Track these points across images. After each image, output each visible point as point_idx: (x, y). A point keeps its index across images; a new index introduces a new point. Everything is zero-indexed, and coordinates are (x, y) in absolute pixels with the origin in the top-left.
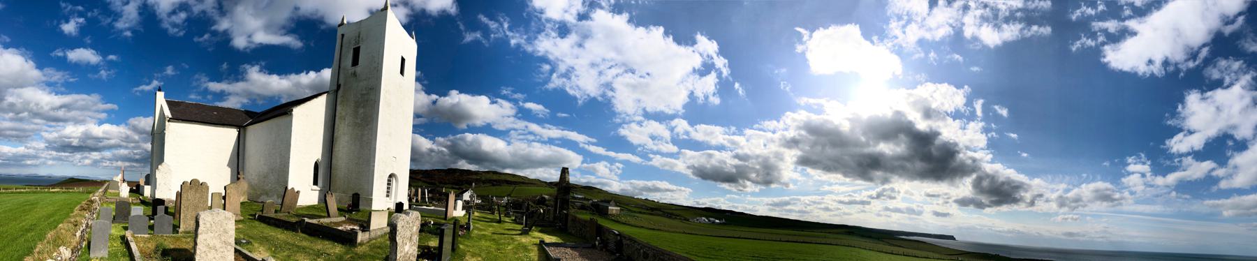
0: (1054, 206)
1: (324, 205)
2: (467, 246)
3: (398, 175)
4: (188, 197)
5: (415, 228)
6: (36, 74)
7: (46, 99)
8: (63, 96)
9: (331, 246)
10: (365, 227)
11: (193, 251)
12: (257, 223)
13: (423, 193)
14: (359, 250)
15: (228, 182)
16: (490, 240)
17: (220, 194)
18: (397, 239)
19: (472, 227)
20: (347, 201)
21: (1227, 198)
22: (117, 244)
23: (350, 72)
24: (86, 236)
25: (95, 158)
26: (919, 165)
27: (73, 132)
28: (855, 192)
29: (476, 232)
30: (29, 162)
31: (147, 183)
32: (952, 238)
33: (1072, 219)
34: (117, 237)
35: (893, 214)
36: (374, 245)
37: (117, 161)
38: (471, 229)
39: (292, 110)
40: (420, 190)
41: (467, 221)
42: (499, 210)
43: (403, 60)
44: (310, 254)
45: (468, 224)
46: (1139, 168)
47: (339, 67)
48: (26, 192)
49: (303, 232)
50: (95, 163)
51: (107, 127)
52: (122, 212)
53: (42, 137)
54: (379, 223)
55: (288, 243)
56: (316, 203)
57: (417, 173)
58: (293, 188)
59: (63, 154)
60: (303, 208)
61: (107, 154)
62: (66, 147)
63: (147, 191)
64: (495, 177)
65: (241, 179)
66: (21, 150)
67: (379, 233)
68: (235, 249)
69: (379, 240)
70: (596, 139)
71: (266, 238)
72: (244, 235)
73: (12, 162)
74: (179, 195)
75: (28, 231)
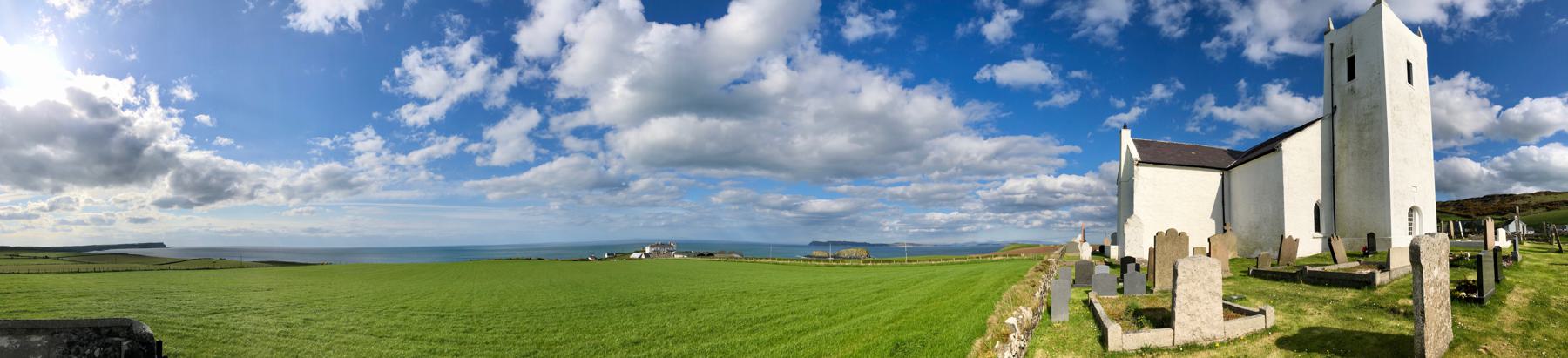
0: (281, 198)
3: (1421, 208)
4: (1166, 248)
6: (956, 115)
7: (975, 148)
8: (996, 139)
10: (1385, 267)
11: (1170, 310)
12: (1251, 279)
13: (1456, 226)
14: (1379, 292)
15: (1213, 232)
16: (1547, 272)
17: (1203, 249)
20: (1363, 242)
21: (487, 179)
22: (1079, 308)
24: (1045, 300)
25: (1049, 218)
26: (101, 169)
27: (1019, 186)
28: (16, 203)
29: (1526, 262)
30: (964, 229)
31: (1114, 242)
32: (161, 245)
33: (308, 212)
34: (1078, 301)
35: (73, 227)
36: (1398, 288)
37: (1078, 221)
38: (1519, 260)
40: (1452, 223)
41: (1512, 250)
42: (1557, 239)
44: (1313, 302)
46: (370, 144)
48: (968, 263)
49: (1305, 282)
50: (1048, 224)
51: (1064, 179)
52: (1083, 275)
53: (978, 197)
54: (1400, 261)
55: (1290, 294)
56: (1320, 252)
58: (1290, 237)
59: (1002, 215)
60: (1303, 259)
61: (1065, 213)
62: (1008, 205)
63: (1114, 252)
64: (1549, 199)
65: (1228, 232)
66: (955, 214)
67: (1402, 273)
68: (1224, 304)
70: (1081, 146)
71: (1263, 292)
72: (1235, 291)
73: (947, 231)
74: (1153, 252)
75: (979, 300)
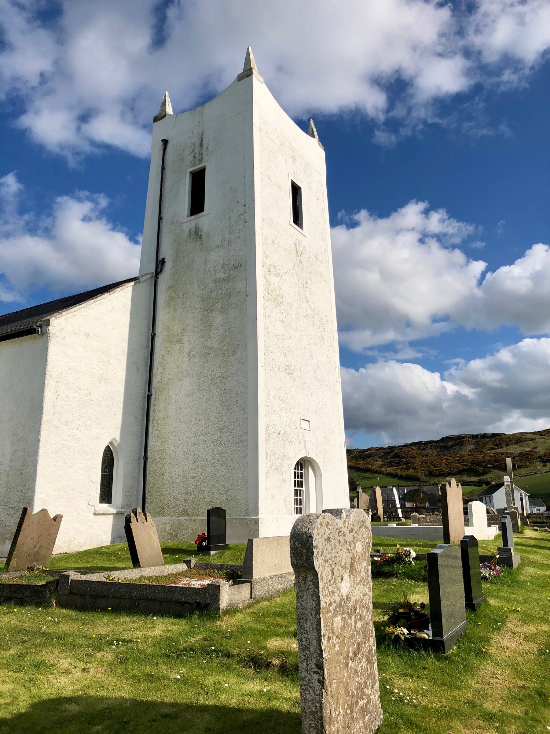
1: (126, 545)
2: (508, 601)
5: (359, 547)
9: (141, 623)
18: (316, 564)
19: (516, 559)
23: (186, 228)
29: (531, 570)
39: (48, 323)
40: (378, 491)
43: (296, 190)
45: (505, 551)
47: (160, 219)
49: (62, 605)
56: (109, 544)
57: (369, 456)
58: (44, 511)
60: (67, 557)
69: (278, 600)
